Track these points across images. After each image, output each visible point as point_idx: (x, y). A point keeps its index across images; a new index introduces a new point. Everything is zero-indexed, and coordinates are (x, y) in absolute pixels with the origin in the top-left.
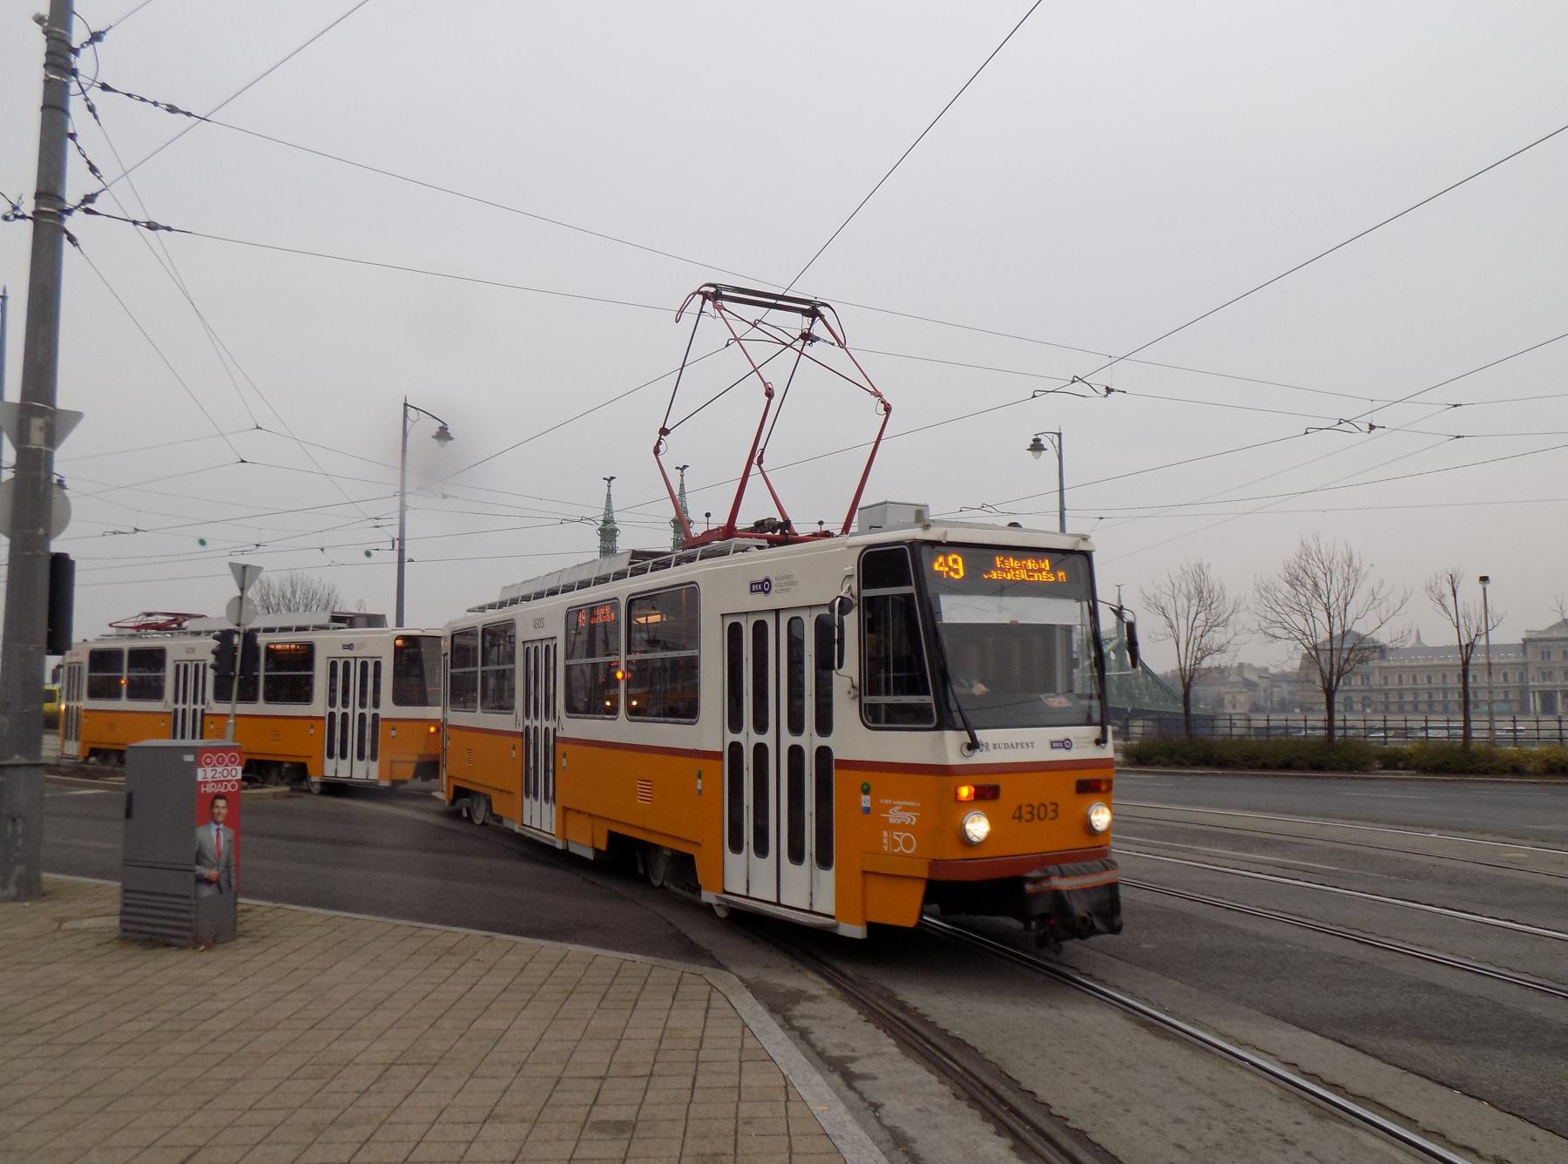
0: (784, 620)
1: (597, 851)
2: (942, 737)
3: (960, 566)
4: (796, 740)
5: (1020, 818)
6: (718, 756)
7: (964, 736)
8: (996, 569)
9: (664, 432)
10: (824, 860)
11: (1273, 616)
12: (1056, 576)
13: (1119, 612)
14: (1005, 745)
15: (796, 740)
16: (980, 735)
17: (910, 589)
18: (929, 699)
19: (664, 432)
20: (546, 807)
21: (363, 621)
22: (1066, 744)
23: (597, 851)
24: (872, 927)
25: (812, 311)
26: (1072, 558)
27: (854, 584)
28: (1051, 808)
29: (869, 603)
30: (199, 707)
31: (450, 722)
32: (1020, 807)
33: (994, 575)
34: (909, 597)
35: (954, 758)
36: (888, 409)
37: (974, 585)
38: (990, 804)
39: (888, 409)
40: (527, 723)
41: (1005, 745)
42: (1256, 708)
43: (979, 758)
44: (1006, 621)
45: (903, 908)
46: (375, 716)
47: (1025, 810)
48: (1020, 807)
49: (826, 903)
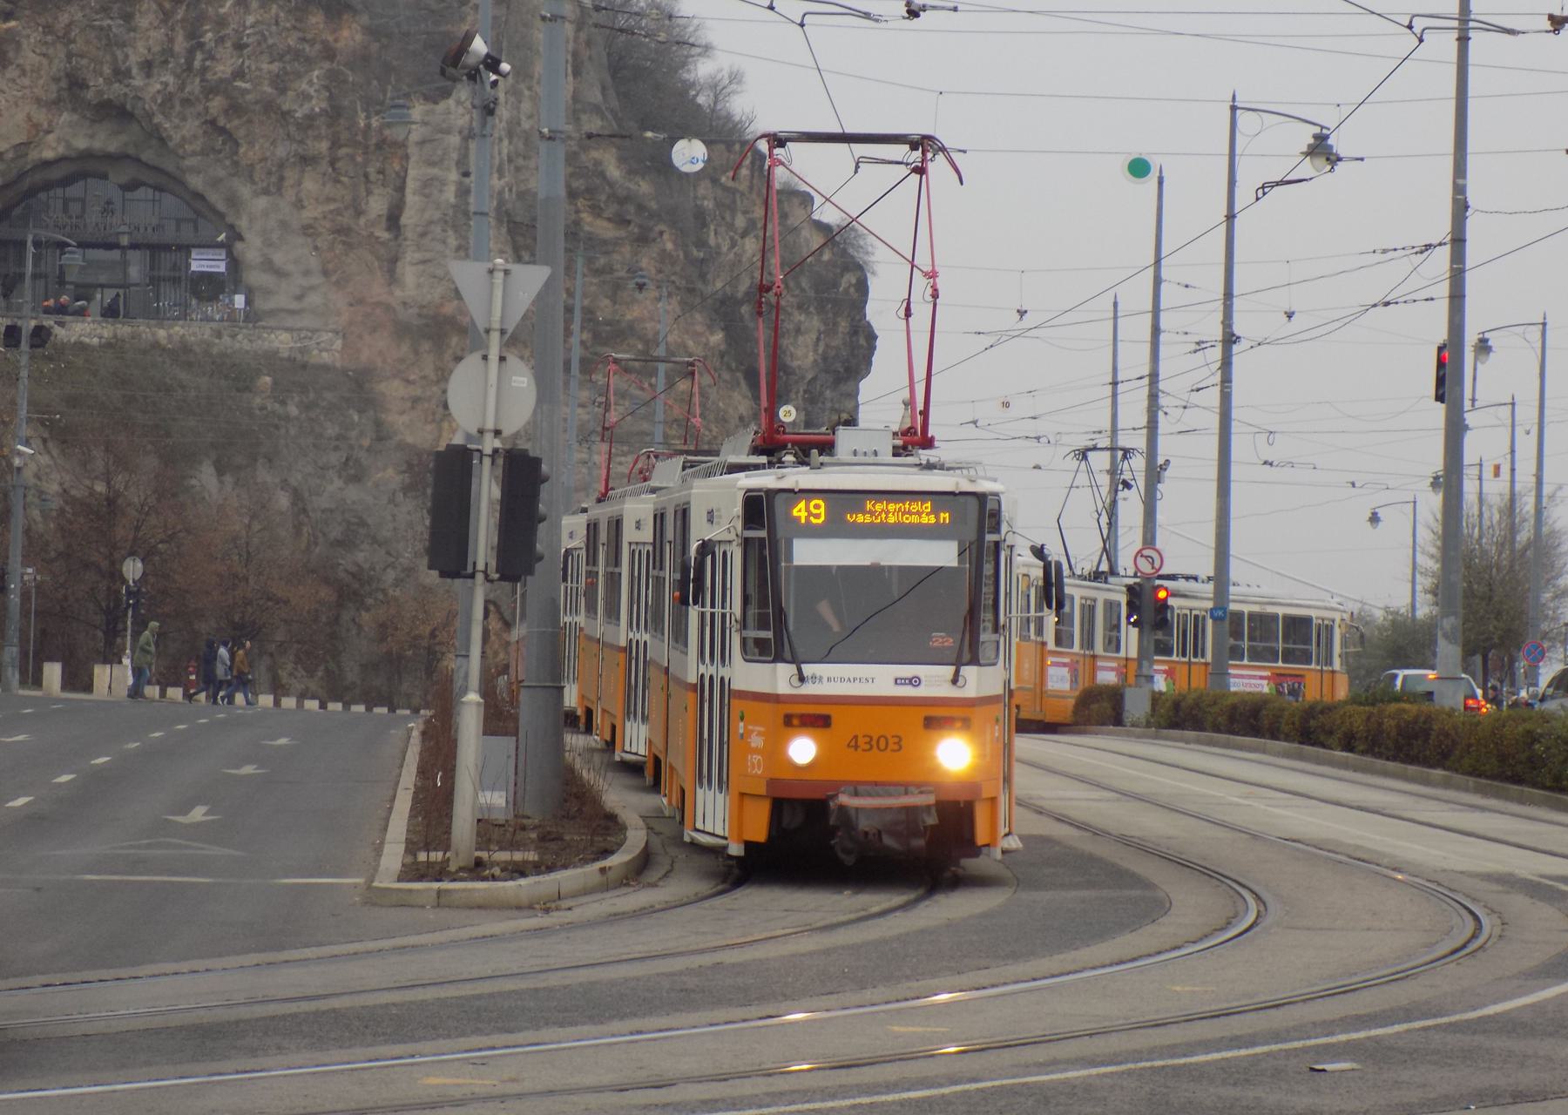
1: (749, 845)
2: (775, 671)
3: (822, 511)
5: (856, 747)
7: (792, 668)
8: (864, 513)
12: (937, 517)
13: (1039, 552)
14: (833, 679)
16: (808, 669)
17: (763, 534)
20: (720, 797)
21: (1460, 181)
22: (914, 681)
23: (749, 845)
26: (962, 499)
27: (739, 525)
28: (891, 741)
29: (746, 543)
31: (737, 685)
32: (856, 737)
33: (860, 518)
34: (762, 540)
35: (783, 688)
37: (836, 528)
38: (820, 731)
40: (702, 669)
41: (833, 679)
43: (809, 689)
44: (867, 563)
47: (860, 739)
48: (856, 737)
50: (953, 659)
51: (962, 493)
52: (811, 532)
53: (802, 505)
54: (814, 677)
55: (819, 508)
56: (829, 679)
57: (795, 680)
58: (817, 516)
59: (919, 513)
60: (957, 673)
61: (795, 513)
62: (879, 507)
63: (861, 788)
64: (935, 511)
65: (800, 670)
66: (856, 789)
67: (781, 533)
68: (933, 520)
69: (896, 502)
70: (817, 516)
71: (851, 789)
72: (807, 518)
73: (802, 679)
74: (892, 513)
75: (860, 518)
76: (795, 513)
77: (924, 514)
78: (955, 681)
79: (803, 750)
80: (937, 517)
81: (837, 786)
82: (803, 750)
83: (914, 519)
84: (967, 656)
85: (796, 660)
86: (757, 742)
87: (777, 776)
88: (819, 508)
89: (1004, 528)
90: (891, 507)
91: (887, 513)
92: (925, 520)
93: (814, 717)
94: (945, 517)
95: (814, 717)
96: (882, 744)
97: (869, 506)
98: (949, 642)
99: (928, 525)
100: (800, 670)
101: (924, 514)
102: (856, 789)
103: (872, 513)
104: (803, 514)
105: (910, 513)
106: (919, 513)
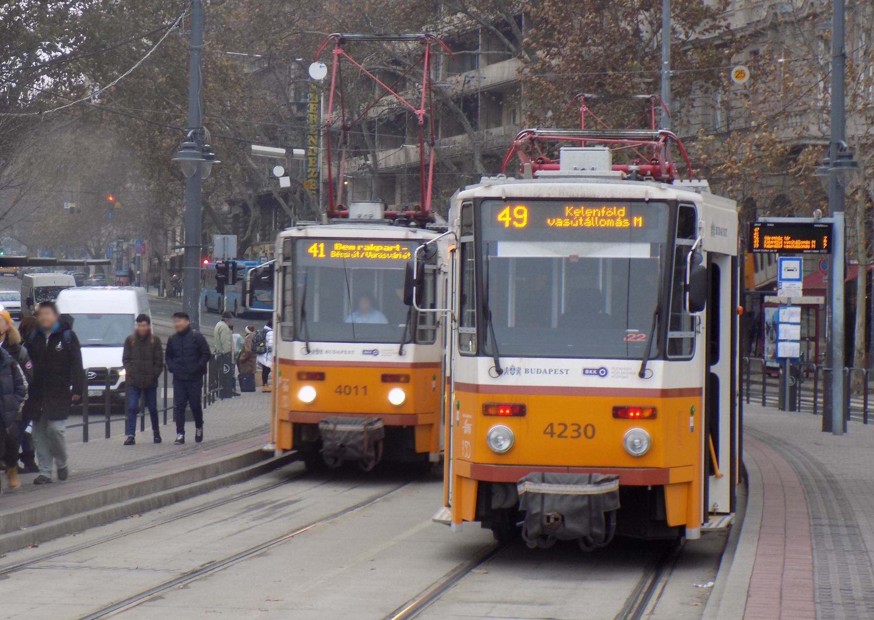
3: (525, 216)
5: (552, 434)
7: (303, 344)
8: (563, 217)
12: (631, 221)
14: (328, 352)
16: (313, 345)
22: (374, 352)
32: (551, 425)
33: (559, 223)
37: (535, 232)
48: (551, 425)
50: (400, 340)
51: (652, 200)
52: (514, 235)
53: (507, 211)
54: (512, 369)
55: (522, 215)
56: (527, 371)
57: (494, 372)
58: (520, 221)
59: (614, 218)
60: (401, 347)
61: (500, 218)
62: (577, 212)
63: (548, 475)
64: (630, 216)
65: (497, 363)
66: (545, 472)
67: (486, 237)
68: (626, 223)
69: (593, 207)
70: (520, 221)
71: (539, 474)
72: (511, 223)
73: (499, 371)
74: (589, 217)
75: (559, 223)
76: (500, 218)
77: (618, 218)
78: (642, 375)
79: (307, 394)
80: (631, 221)
81: (526, 470)
82: (307, 394)
83: (609, 223)
84: (654, 351)
85: (496, 356)
86: (467, 428)
87: (477, 461)
88: (522, 213)
89: (439, 262)
90: (589, 212)
91: (585, 218)
92: (619, 223)
93: (315, 375)
94: (638, 221)
95: (315, 375)
96: (347, 391)
97: (568, 210)
98: (643, 338)
99: (621, 228)
100: (497, 363)
101: (618, 218)
102: (545, 472)
103: (571, 218)
104: (507, 220)
105: (606, 217)
106: (614, 218)
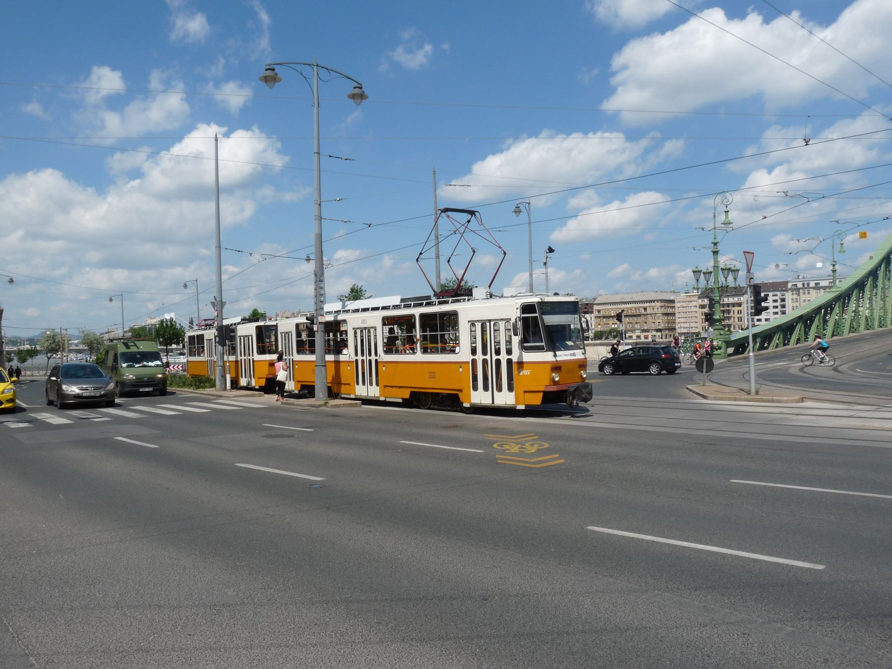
0: (492, 323)
4: (498, 357)
6: (468, 363)
9: (421, 254)
10: (377, 384)
11: (727, 322)
15: (498, 357)
16: (557, 353)
18: (543, 344)
19: (421, 254)
22: (574, 355)
24: (526, 406)
25: (472, 213)
30: (291, 357)
36: (505, 253)
39: (505, 253)
42: (125, 332)
45: (537, 400)
46: (376, 360)
49: (377, 394)
